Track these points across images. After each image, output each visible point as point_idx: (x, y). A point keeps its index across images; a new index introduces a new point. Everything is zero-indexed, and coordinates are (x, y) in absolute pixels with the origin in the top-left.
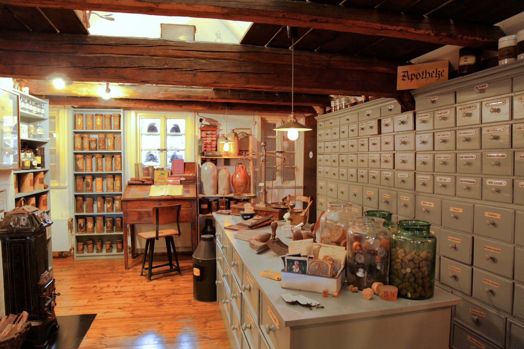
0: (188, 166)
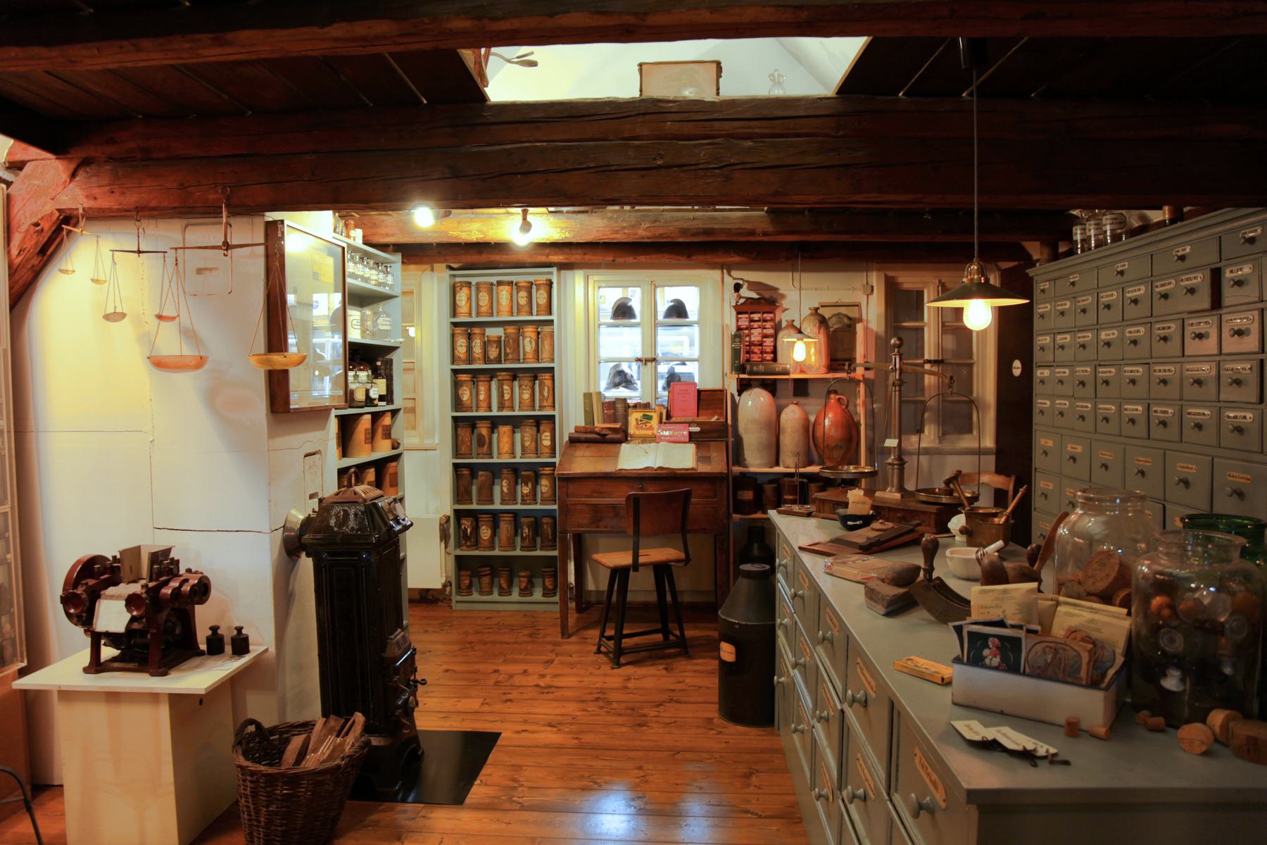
0: (708, 399)
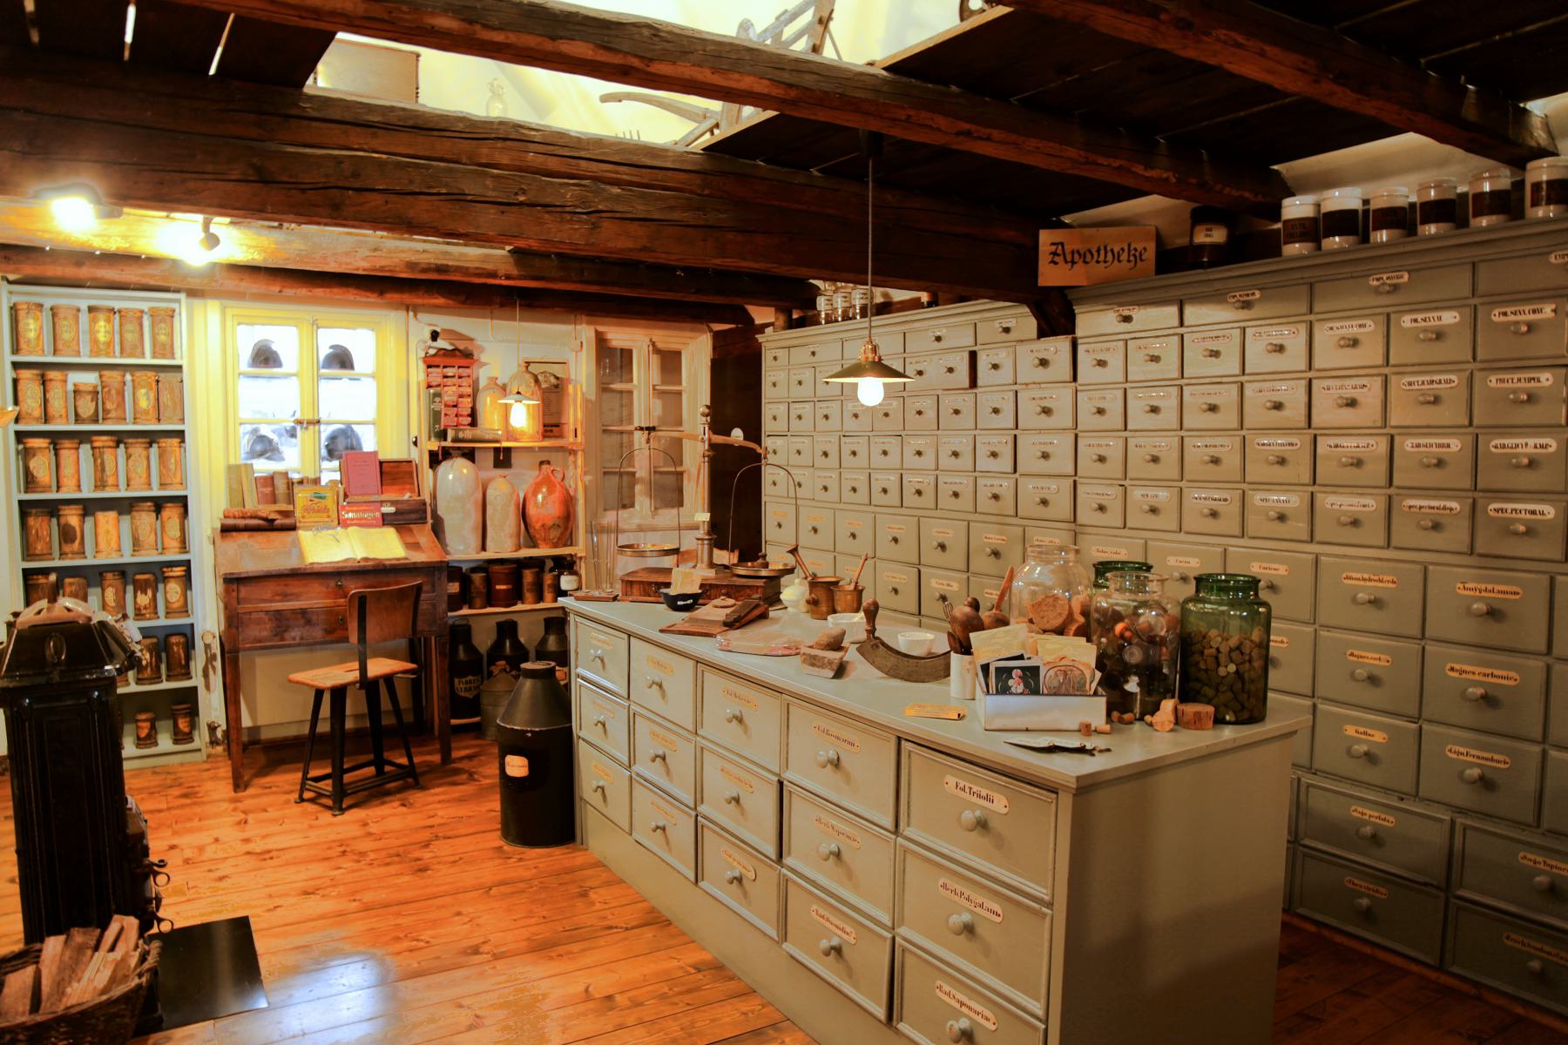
0: (393, 472)
